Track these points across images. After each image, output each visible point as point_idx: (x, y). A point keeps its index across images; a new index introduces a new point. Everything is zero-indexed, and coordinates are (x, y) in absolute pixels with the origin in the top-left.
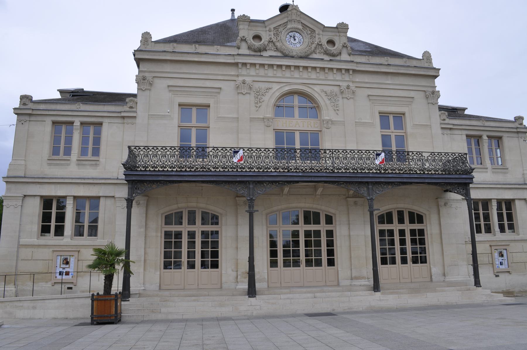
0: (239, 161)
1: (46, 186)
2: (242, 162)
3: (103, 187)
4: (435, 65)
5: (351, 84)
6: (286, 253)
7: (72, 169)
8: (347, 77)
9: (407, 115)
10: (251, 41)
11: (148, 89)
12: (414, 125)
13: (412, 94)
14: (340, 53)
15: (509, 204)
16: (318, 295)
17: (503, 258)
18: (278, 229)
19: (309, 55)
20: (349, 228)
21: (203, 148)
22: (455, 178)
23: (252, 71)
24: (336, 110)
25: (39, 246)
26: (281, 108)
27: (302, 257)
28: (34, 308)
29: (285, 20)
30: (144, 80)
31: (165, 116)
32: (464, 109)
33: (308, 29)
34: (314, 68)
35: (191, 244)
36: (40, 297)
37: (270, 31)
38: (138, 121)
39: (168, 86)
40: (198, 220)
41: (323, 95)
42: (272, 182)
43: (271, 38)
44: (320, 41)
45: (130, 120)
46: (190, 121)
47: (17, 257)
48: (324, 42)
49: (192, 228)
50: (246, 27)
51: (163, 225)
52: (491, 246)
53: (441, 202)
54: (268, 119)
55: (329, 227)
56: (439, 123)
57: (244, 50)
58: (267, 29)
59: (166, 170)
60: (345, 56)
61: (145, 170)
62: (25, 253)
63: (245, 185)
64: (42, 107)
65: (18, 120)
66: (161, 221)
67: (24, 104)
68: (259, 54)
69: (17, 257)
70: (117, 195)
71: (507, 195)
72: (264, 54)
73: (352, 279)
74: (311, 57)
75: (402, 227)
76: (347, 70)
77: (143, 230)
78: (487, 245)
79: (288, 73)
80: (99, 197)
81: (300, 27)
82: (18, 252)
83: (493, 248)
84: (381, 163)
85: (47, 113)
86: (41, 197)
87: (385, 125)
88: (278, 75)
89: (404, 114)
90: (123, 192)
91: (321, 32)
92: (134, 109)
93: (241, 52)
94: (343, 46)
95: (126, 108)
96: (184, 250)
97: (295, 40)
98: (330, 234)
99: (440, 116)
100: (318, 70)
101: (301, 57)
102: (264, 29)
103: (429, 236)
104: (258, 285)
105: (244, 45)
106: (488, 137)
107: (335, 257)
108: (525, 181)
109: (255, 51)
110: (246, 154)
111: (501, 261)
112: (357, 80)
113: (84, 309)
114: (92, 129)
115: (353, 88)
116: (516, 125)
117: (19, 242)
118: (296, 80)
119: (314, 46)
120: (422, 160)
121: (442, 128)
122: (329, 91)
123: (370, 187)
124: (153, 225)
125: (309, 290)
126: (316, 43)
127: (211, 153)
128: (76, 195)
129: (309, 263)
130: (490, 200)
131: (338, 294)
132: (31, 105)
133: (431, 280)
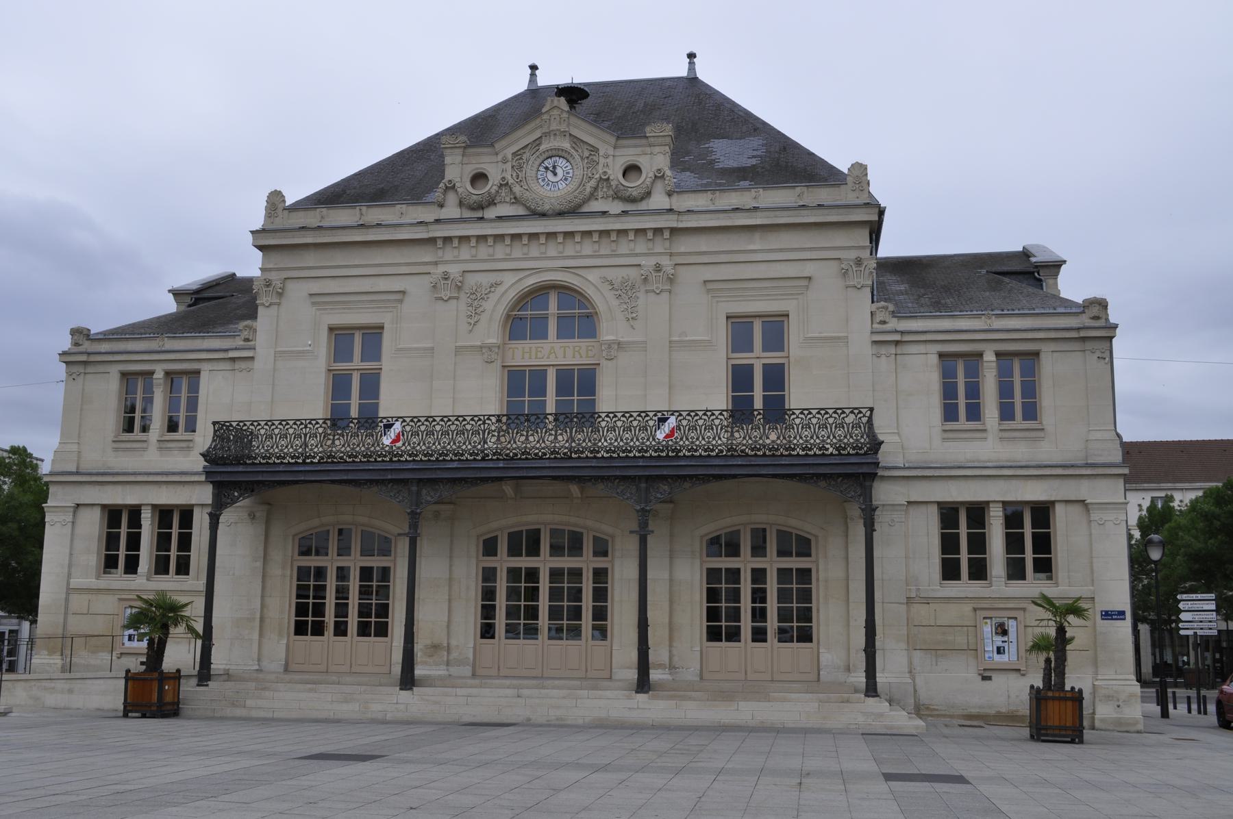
0: (394, 441)
2: (399, 444)
5: (665, 261)
8: (660, 246)
12: (806, 339)
13: (808, 269)
15: (1042, 512)
16: (525, 692)
17: (1005, 639)
18: (584, 566)
19: (580, 206)
23: (465, 252)
24: (631, 318)
25: (99, 591)
26: (523, 319)
27: (543, 620)
28: (70, 691)
29: (537, 134)
30: (268, 286)
31: (303, 352)
34: (588, 233)
36: (78, 675)
37: (505, 161)
38: (257, 364)
40: (772, 546)
41: (605, 288)
43: (503, 179)
45: (243, 365)
47: (66, 608)
48: (616, 173)
49: (759, 563)
51: (296, 556)
52: (975, 610)
54: (490, 348)
55: (600, 563)
58: (500, 158)
60: (659, 200)
62: (78, 602)
63: (434, 483)
64: (105, 347)
65: (69, 374)
66: (291, 548)
69: (66, 608)
72: (491, 213)
74: (585, 209)
76: (658, 231)
77: (259, 564)
78: (967, 608)
81: (566, 145)
82: (67, 600)
85: (110, 358)
86: (939, 503)
88: (584, 253)
90: (203, 495)
91: (611, 151)
93: (445, 213)
96: (746, 604)
97: (555, 174)
98: (601, 575)
102: (494, 159)
103: (821, 584)
109: (472, 208)
111: (1000, 644)
112: (682, 249)
113: (112, 695)
114: (184, 383)
115: (670, 270)
116: (1085, 320)
117: (68, 583)
119: (593, 183)
121: (875, 342)
122: (620, 279)
124: (277, 556)
125: (508, 682)
131: (565, 692)
132: (87, 346)
133: (819, 680)
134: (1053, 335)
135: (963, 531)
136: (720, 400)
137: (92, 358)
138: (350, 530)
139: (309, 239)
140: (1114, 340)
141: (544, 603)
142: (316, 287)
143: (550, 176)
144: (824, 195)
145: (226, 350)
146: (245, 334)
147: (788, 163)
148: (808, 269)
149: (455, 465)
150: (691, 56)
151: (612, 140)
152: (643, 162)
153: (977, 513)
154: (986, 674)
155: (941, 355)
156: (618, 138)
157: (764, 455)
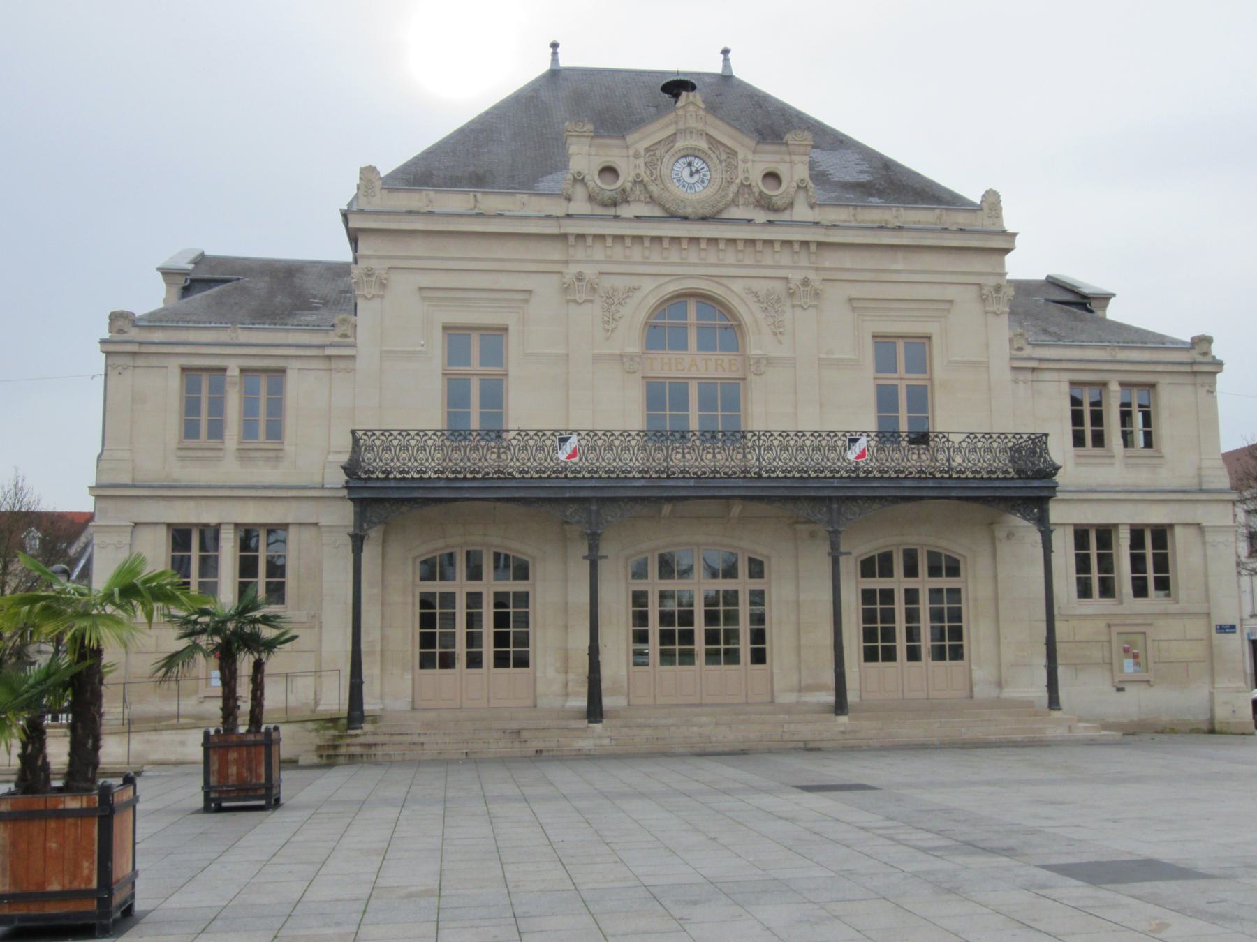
0: (570, 457)
1: (179, 505)
2: (576, 460)
3: (294, 504)
4: (1009, 226)
5: (812, 275)
6: (666, 637)
7: (228, 468)
8: (803, 260)
9: (935, 340)
10: (595, 181)
11: (378, 296)
13: (951, 293)
14: (792, 204)
15: (1161, 535)
19: (720, 211)
20: (797, 587)
21: (498, 431)
22: (1023, 488)
23: (598, 252)
26: (662, 329)
27: (700, 645)
29: (671, 131)
30: (369, 275)
32: (1105, 298)
33: (722, 149)
34: (732, 241)
35: (473, 620)
37: (637, 156)
39: (421, 289)
42: (635, 500)
43: (638, 175)
44: (747, 179)
45: (342, 364)
46: (468, 364)
48: (756, 176)
50: (586, 148)
52: (1109, 626)
53: (1001, 533)
54: (631, 358)
55: (756, 584)
56: (1007, 357)
57: (580, 206)
58: (631, 152)
59: (426, 476)
60: (801, 212)
61: (387, 479)
63: (583, 505)
64: (158, 336)
67: (121, 331)
68: (611, 211)
70: (324, 521)
71: (1156, 516)
72: (626, 211)
73: (800, 690)
74: (725, 215)
75: (911, 583)
76: (805, 244)
78: (1102, 624)
79: (674, 255)
80: (285, 527)
81: (703, 144)
83: (1115, 630)
84: (858, 457)
86: (169, 525)
87: (885, 362)
88: (727, 262)
89: (929, 338)
91: (750, 156)
92: (351, 340)
94: (799, 187)
95: (333, 337)
96: (900, 625)
98: (758, 598)
99: (1011, 340)
100: (740, 246)
101: (704, 219)
104: (607, 702)
105: (580, 192)
106: (1122, 384)
107: (862, 644)
108: (1200, 483)
110: (583, 443)
112: (827, 264)
116: (1194, 355)
118: (690, 270)
119: (734, 188)
120: (949, 449)
121: (1014, 369)
123: (835, 506)
126: (738, 181)
127: (514, 442)
128: (239, 521)
129: (712, 657)
130: (1116, 526)
132: (134, 334)
133: (971, 697)
134: (1170, 368)
135: (1093, 551)
136: (868, 422)
137: (144, 349)
138: (481, 552)
139: (419, 225)
140: (1218, 376)
141: (699, 627)
142: (427, 280)
143: (686, 172)
144: (961, 219)
145: (322, 347)
146: (341, 329)
147: (892, 184)
148: (951, 293)
149: (642, 483)
150: (726, 52)
151: (752, 144)
152: (782, 170)
153: (1105, 534)
154: (1120, 686)
155: (184, 369)
156: (758, 143)
157: (950, 478)
